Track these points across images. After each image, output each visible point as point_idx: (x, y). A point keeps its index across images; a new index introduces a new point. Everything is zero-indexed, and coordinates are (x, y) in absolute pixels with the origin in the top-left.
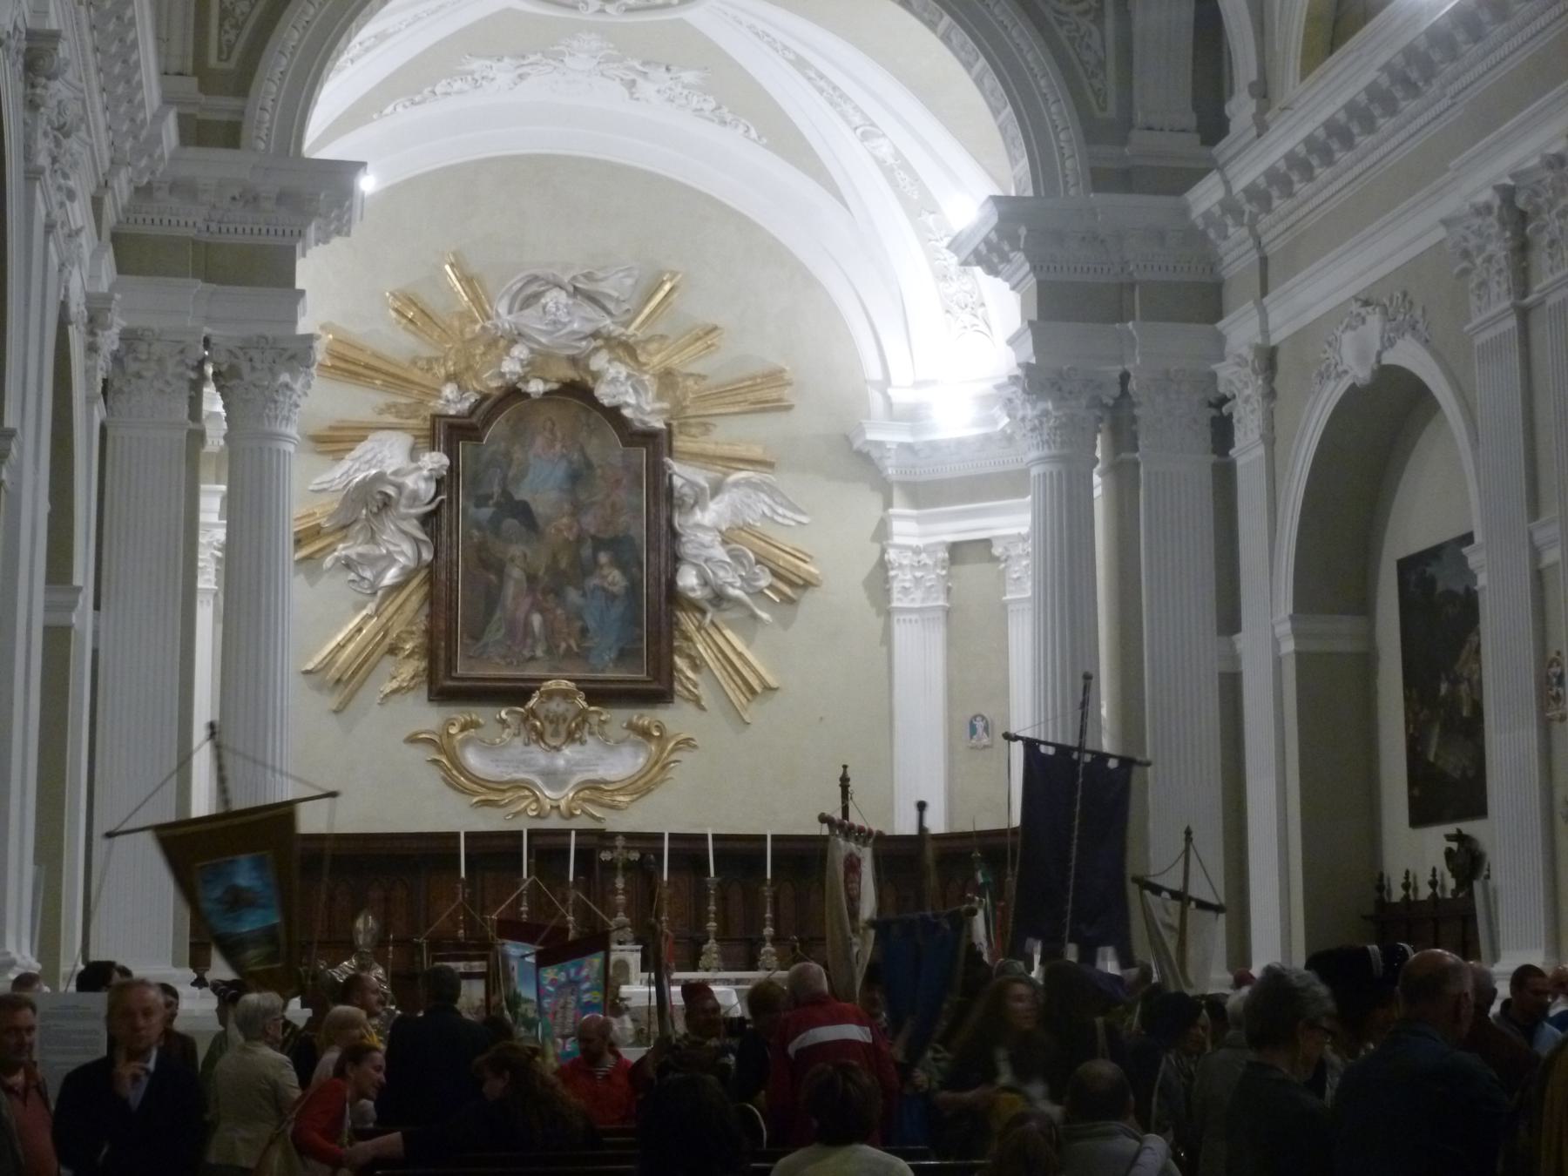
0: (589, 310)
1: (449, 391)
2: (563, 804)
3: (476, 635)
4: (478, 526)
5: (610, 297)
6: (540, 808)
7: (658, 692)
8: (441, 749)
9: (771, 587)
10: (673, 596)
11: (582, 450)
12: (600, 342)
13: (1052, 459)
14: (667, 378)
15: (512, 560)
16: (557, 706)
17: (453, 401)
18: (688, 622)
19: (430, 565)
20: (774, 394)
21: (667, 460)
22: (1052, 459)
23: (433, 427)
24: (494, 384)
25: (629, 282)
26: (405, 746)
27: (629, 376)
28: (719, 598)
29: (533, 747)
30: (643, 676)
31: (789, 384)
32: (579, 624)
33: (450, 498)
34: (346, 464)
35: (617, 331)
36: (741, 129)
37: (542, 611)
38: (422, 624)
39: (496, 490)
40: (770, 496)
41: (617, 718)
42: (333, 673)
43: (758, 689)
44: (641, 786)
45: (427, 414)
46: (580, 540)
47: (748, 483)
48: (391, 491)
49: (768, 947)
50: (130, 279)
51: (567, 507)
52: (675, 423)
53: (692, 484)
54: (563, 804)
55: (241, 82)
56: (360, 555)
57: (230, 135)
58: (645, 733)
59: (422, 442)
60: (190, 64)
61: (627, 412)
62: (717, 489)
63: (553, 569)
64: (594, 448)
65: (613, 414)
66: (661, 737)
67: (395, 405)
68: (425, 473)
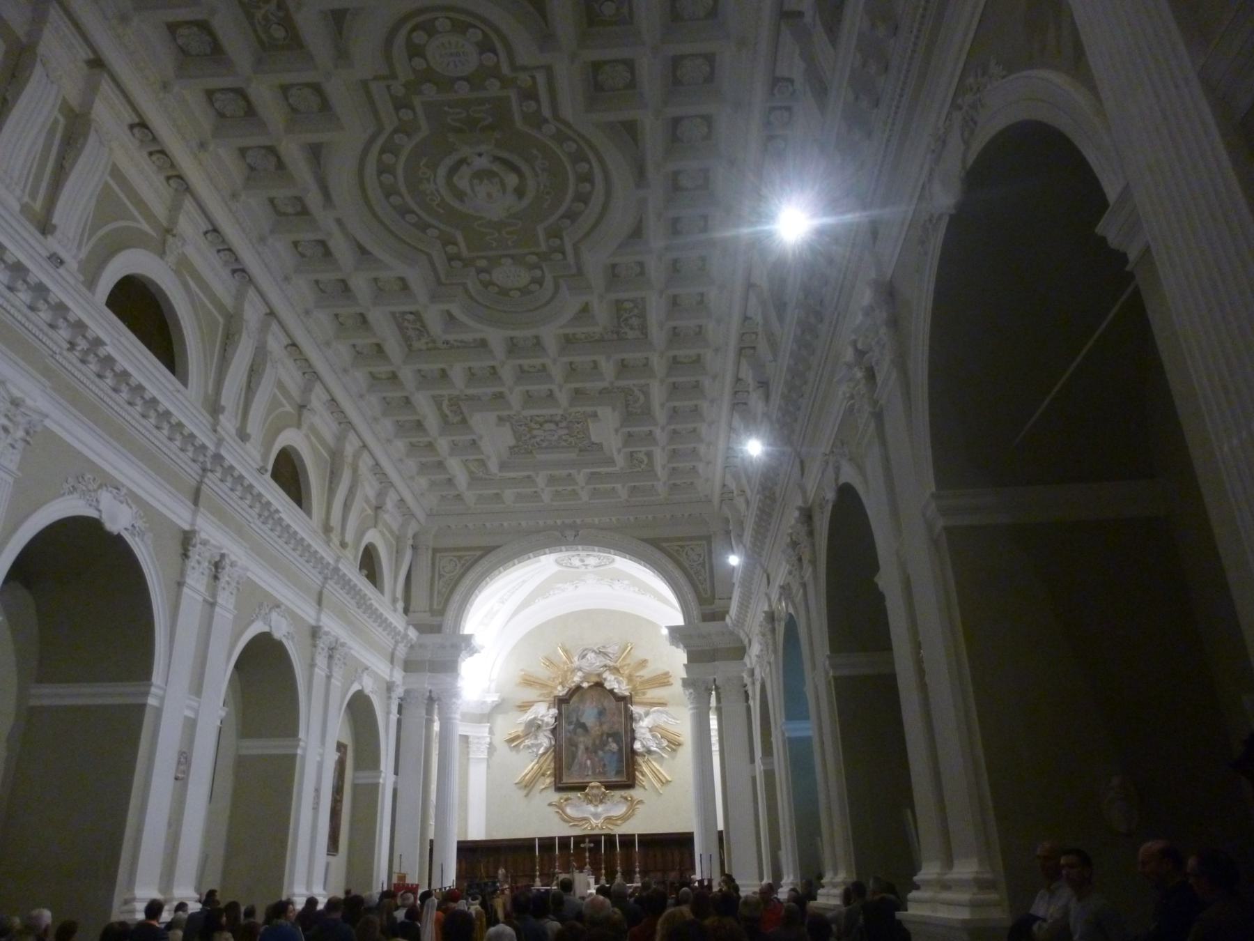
0: (601, 658)
1: (560, 688)
2: (599, 825)
3: (569, 768)
4: (569, 732)
5: (610, 653)
6: (592, 826)
7: (630, 784)
8: (559, 808)
9: (667, 746)
10: (633, 752)
11: (602, 704)
12: (607, 668)
13: (694, 708)
14: (630, 679)
15: (580, 742)
16: (595, 791)
17: (561, 691)
18: (640, 760)
19: (554, 746)
20: (666, 681)
21: (630, 706)
22: (694, 708)
23: (555, 700)
24: (573, 685)
25: (617, 647)
26: (548, 807)
27: (615, 679)
28: (649, 752)
29: (589, 806)
30: (625, 779)
31: (671, 676)
32: (602, 763)
33: (559, 723)
34: (526, 715)
35: (612, 664)
36: (648, 596)
37: (590, 759)
38: (552, 765)
39: (575, 719)
40: (667, 715)
41: (618, 794)
42: (524, 783)
43: (664, 781)
44: (625, 818)
45: (552, 696)
46: (602, 735)
47: (658, 711)
48: (540, 722)
49: (638, 875)
50: (408, 674)
51: (598, 723)
52: (633, 693)
53: (638, 713)
54: (599, 825)
55: (442, 612)
56: (532, 744)
57: (437, 629)
58: (626, 799)
59: (552, 705)
60: (427, 609)
61: (616, 691)
62: (647, 714)
63: (594, 744)
64: (606, 703)
65: (611, 691)
66: (631, 801)
67: (544, 694)
68: (550, 716)
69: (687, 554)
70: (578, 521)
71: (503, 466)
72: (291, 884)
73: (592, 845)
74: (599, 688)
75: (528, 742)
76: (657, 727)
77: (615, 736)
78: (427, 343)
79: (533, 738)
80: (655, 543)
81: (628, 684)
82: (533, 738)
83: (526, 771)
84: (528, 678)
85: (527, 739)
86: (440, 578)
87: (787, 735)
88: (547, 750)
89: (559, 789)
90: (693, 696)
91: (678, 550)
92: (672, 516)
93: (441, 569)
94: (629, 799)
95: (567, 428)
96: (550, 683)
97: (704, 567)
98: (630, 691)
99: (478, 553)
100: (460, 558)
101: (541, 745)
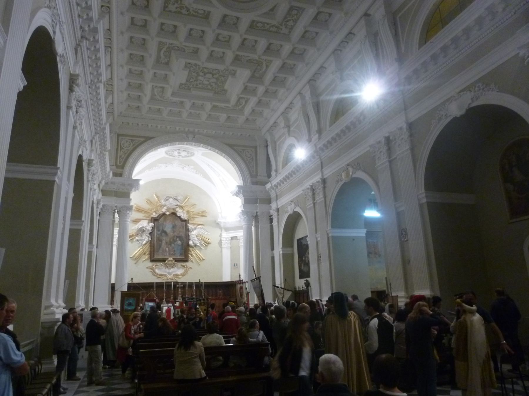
0: (176, 202)
1: (154, 214)
2: (171, 278)
7: (186, 260)
9: (204, 244)
10: (188, 245)
12: (178, 206)
14: (188, 212)
16: (170, 262)
18: (191, 249)
19: (150, 241)
20: (204, 214)
24: (161, 213)
25: (182, 197)
27: (182, 212)
28: (196, 246)
29: (167, 269)
30: (184, 258)
31: (207, 213)
33: (154, 230)
34: (138, 225)
35: (180, 205)
37: (168, 248)
38: (149, 250)
39: (161, 229)
41: (180, 264)
44: (183, 275)
45: (150, 217)
46: (174, 237)
47: (200, 228)
48: (145, 229)
50: (104, 197)
51: (172, 231)
55: (123, 167)
56: (140, 239)
58: (184, 266)
60: (114, 165)
61: (182, 217)
62: (195, 229)
65: (179, 217)
68: (150, 226)
69: (245, 153)
70: (196, 130)
71: (174, 94)
72: (78, 302)
73: (182, 286)
74: (173, 215)
75: (137, 238)
76: (199, 235)
77: (180, 238)
78: (176, 8)
79: (140, 236)
80: (231, 146)
81: (187, 215)
82: (140, 236)
83: (136, 252)
84: (138, 207)
85: (137, 237)
86: (121, 150)
87: (330, 235)
88: (147, 242)
89: (152, 260)
90: (246, 219)
91: (241, 152)
92: (241, 135)
93: (122, 145)
94: (186, 266)
95: (217, 79)
96: (149, 211)
97: (253, 160)
98: (187, 218)
99: (143, 140)
100: (132, 141)
101: (144, 240)
